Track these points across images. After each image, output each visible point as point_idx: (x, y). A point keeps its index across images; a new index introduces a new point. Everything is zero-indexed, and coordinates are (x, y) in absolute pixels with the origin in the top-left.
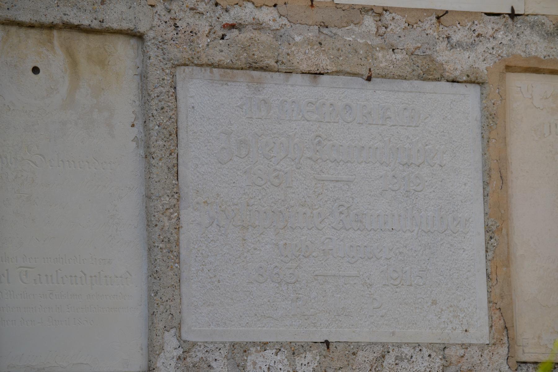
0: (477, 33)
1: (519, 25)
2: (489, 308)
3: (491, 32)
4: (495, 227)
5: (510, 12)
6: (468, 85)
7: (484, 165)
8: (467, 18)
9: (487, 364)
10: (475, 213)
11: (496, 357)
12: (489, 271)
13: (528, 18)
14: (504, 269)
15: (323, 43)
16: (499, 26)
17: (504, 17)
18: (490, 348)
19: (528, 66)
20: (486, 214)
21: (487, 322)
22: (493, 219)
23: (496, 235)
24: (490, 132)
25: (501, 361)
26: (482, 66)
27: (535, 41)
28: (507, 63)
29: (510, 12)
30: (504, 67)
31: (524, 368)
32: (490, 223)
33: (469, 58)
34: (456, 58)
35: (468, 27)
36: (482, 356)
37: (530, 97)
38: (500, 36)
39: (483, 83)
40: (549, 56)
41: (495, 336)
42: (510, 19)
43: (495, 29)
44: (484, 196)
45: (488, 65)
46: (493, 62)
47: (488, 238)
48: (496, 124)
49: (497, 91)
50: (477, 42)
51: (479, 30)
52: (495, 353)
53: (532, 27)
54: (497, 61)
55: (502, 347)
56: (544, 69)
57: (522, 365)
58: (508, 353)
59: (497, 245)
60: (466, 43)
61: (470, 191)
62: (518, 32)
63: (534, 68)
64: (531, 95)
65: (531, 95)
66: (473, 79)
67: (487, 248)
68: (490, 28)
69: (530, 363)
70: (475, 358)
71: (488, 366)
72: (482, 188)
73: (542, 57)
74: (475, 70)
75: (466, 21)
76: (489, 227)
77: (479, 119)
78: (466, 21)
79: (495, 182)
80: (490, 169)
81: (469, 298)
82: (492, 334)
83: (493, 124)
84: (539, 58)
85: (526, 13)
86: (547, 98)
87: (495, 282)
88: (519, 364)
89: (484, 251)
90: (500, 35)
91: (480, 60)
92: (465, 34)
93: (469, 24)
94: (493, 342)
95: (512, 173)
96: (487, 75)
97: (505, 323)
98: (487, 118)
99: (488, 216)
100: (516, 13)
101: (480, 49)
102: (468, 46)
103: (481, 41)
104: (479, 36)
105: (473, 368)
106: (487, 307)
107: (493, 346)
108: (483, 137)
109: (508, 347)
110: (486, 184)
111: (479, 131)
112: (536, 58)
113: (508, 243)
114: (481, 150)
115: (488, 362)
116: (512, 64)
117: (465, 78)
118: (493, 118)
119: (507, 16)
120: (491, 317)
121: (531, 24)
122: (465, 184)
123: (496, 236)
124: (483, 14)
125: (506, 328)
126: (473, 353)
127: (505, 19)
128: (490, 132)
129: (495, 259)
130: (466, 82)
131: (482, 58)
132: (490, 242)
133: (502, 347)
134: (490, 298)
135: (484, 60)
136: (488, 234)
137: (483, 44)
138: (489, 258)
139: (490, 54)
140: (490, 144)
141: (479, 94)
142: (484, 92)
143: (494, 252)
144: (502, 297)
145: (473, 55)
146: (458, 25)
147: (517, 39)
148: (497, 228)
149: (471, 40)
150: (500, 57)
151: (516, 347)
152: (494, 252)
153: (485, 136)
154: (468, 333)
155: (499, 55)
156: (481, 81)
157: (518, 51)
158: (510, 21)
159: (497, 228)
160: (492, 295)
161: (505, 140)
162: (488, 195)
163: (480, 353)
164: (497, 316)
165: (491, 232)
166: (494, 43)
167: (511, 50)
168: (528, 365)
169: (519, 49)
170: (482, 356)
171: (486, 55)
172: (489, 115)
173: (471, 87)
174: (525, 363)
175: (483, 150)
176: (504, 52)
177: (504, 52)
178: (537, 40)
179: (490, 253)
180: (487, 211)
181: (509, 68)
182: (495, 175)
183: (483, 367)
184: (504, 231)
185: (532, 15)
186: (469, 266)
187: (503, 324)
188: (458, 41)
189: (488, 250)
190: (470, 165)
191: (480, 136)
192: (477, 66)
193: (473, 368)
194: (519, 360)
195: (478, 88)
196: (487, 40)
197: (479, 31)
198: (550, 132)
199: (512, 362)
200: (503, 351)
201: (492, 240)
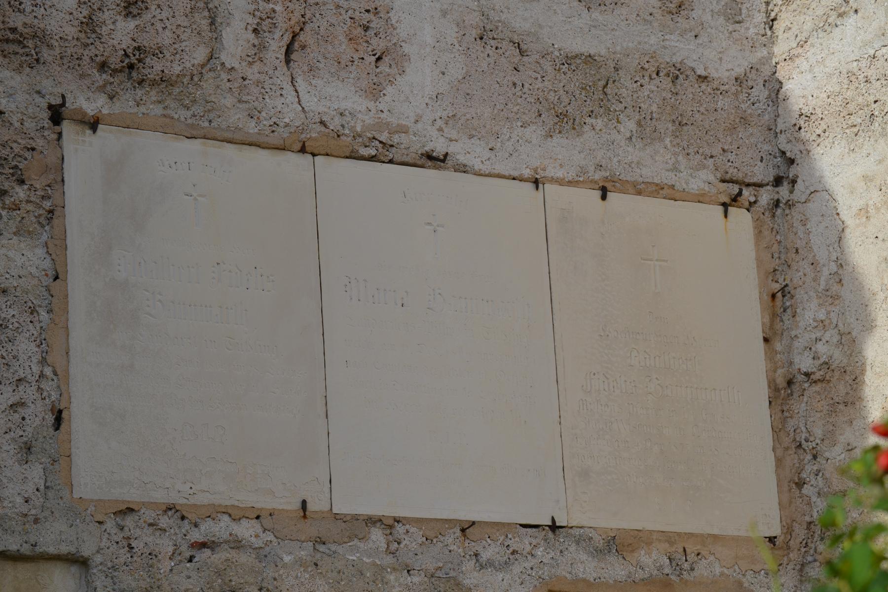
0: (511, 550)
1: (562, 540)
3: (528, 548)
8: (498, 530)
15: (696, 552)
16: (538, 540)
28: (549, 587)
29: (550, 524)
50: (512, 561)
53: (578, 543)
60: (499, 561)
73: (592, 580)
85: (570, 525)
90: (539, 552)
93: (502, 538)
100: (557, 524)
101: (517, 569)
103: (516, 560)
112: (584, 580)
119: (547, 528)
131: (519, 581)
145: (508, 576)
146: (488, 540)
149: (505, 558)
157: (563, 571)
158: (550, 535)
166: (532, 562)
176: (546, 573)
197: (514, 547)
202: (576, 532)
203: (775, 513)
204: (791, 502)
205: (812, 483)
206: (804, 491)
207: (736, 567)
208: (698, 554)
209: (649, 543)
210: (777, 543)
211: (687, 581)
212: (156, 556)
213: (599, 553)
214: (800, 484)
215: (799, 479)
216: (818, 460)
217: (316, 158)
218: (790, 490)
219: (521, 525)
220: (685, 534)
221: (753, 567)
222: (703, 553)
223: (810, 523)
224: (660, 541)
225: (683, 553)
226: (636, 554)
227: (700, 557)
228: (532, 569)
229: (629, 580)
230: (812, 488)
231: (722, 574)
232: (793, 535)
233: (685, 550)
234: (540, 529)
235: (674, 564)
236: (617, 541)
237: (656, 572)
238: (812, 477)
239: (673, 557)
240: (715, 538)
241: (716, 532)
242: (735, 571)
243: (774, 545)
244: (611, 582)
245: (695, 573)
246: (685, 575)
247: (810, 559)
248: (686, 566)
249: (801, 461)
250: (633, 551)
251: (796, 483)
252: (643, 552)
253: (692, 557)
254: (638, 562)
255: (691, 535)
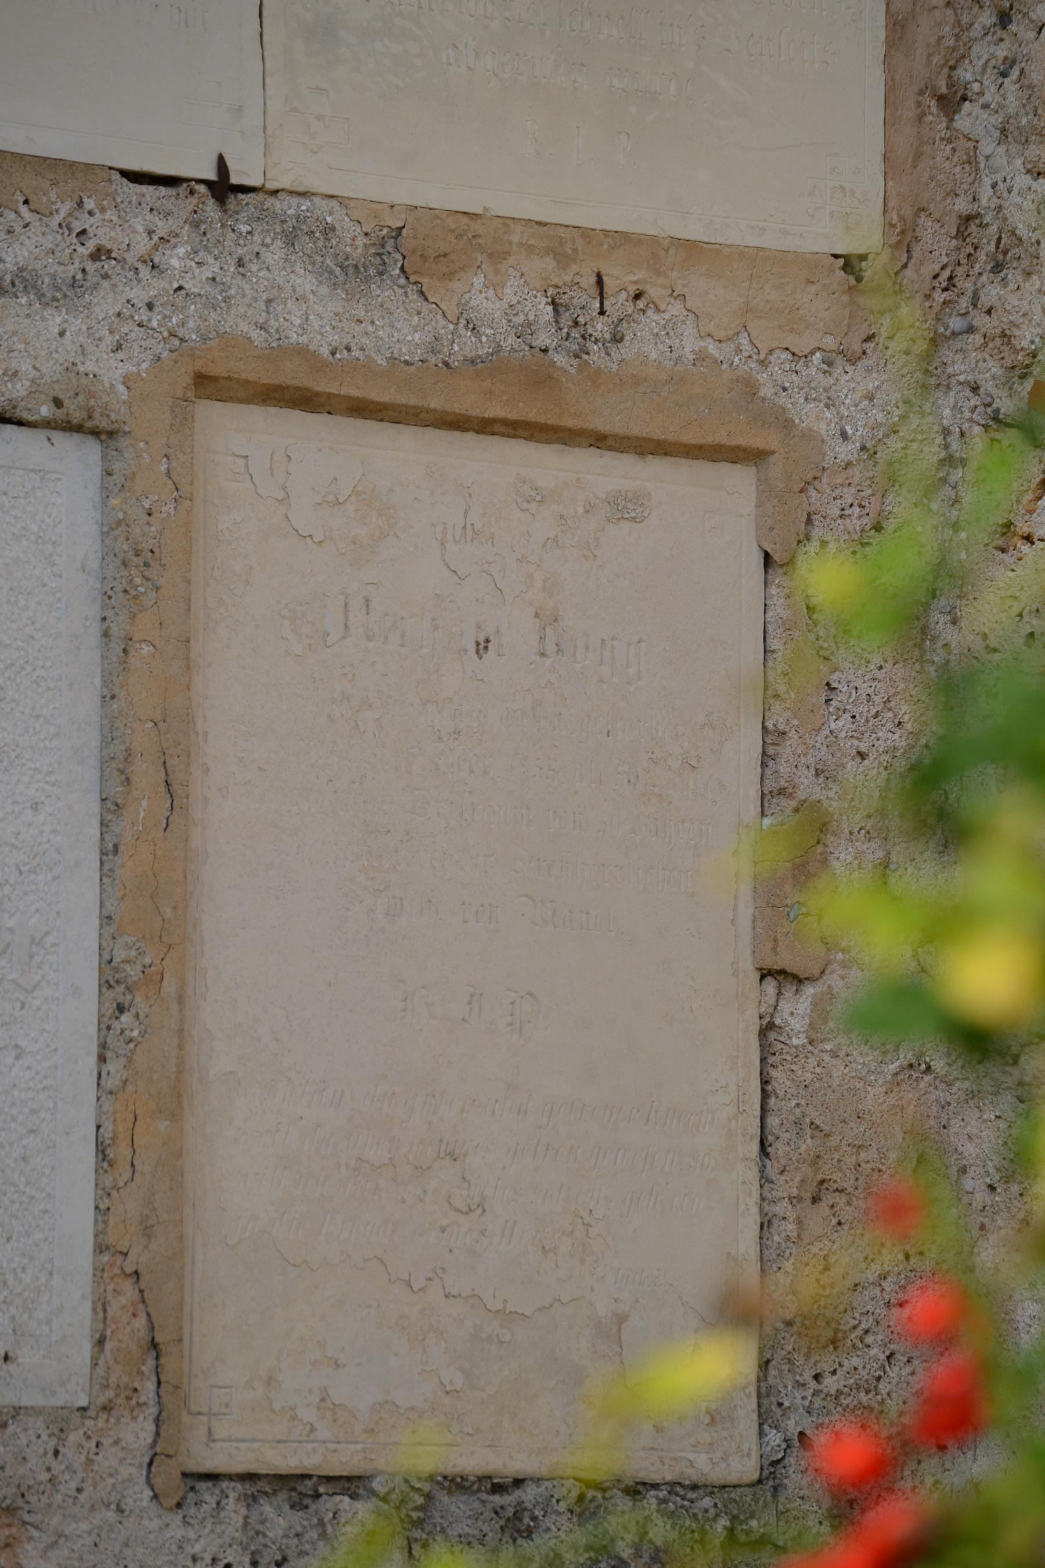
0: (91, 245)
1: (244, 229)
2: (99, 1271)
3: (142, 245)
4: (139, 967)
5: (212, 175)
6: (57, 436)
7: (108, 739)
8: (54, 184)
9: (73, 1485)
10: (69, 918)
11: (109, 1458)
12: (107, 1131)
13: (276, 204)
14: (163, 1125)
15: (632, 290)
16: (173, 224)
17: (192, 192)
18: (90, 1423)
19: (276, 382)
20: (107, 919)
21: (88, 1324)
22: (130, 940)
23: (138, 999)
24: (133, 617)
25: (125, 1471)
26: (111, 371)
27: (300, 291)
28: (199, 365)
29: (212, 175)
30: (188, 380)
31: (207, 1497)
32: (120, 954)
33: (62, 334)
34: (15, 333)
35: (58, 219)
36: (56, 1453)
37: (281, 495)
38: (175, 262)
39: (111, 434)
40: (348, 349)
41: (113, 1379)
42: (211, 201)
43: (160, 233)
44: (103, 853)
45: (130, 368)
46: (149, 356)
47: (110, 1008)
48: (158, 588)
49: (163, 468)
50: (93, 279)
51: (100, 232)
52: (106, 1442)
53: (290, 240)
54: (165, 354)
55: (134, 1419)
56: (330, 396)
57: (202, 1486)
58: (155, 1442)
59: (142, 1034)
60: (54, 277)
61: (54, 832)
62: (240, 251)
63: (297, 389)
64: (284, 487)
65: (284, 487)
66: (77, 417)
67: (103, 1046)
68: (140, 228)
69: (230, 1477)
70: (34, 1461)
71: (79, 1490)
72: (95, 822)
73: (325, 352)
74: (84, 381)
75: (53, 195)
76: (117, 970)
77: (94, 564)
78: (53, 195)
79: (144, 803)
80: (129, 753)
81: (27, 1234)
82: (101, 1371)
83: (146, 584)
84: (315, 355)
85: (271, 186)
86: (338, 503)
87: (128, 1175)
88: (190, 1482)
89: (94, 1058)
90: (175, 259)
91: (103, 346)
92: (48, 243)
93: (65, 208)
94: (102, 1400)
95: (207, 770)
96: (128, 404)
97: (152, 1328)
98: (125, 564)
99: (112, 929)
100: (234, 180)
101: (105, 304)
102: (58, 289)
103: (106, 276)
104: (99, 254)
105: (20, 1502)
106: (89, 1268)
107: (104, 1416)
108: (106, 634)
109: (157, 1421)
110: (111, 809)
111: (95, 611)
112: (302, 351)
113: (181, 1030)
114: (98, 680)
115: (80, 1475)
116: (218, 370)
117: (46, 411)
118: (146, 565)
119: (202, 189)
120: (101, 1306)
121: (288, 226)
122: (35, 807)
123: (141, 1005)
124: (116, 176)
125: (154, 1345)
126: (24, 1441)
127: (193, 201)
128: (133, 617)
129: (130, 1088)
130: (48, 424)
131: (109, 340)
132: (117, 1026)
133: (134, 1419)
134: (104, 1232)
135: (118, 348)
136: (110, 994)
137: (114, 286)
138: (109, 1083)
139: (140, 325)
140: (133, 660)
141: (98, 472)
142: (116, 466)
143: (130, 1060)
144: (147, 1231)
145: (77, 324)
146: (24, 210)
147: (238, 280)
148: (143, 978)
149: (73, 269)
150: (176, 342)
151: (186, 1418)
152: (130, 1060)
153: (114, 631)
154: (11, 1367)
155: (172, 335)
156: (104, 424)
157: (241, 321)
158: (211, 209)
159: (143, 978)
160: (112, 1222)
161: (188, 649)
162: (116, 849)
163: (53, 1442)
164: (123, 1300)
165: (121, 988)
166: (155, 287)
167: (214, 316)
168: (225, 1484)
169: (245, 316)
170: (56, 1453)
171: (125, 329)
172: (130, 555)
173: (66, 444)
174: (213, 1477)
175: (106, 682)
176: (191, 322)
177: (191, 324)
178: (308, 287)
179: (113, 1066)
180: (110, 908)
181: (206, 385)
182: (146, 775)
183: (58, 1498)
184: (169, 986)
185: (291, 193)
186: (33, 1112)
187: (144, 1334)
188: (22, 270)
189: (109, 1054)
190: (57, 735)
191: (96, 628)
192: (90, 367)
193: (20, 1502)
194: (192, 1467)
195: (92, 449)
196: (131, 274)
197: (101, 236)
198: (346, 626)
199: (168, 1475)
200: (138, 1433)
201: (124, 1018)
202: (289, 207)
203: (870, 182)
204: (918, 155)
205: (988, 97)
206: (962, 122)
207: (744, 340)
208: (638, 296)
209: (498, 256)
210: (867, 274)
211: (599, 371)
212: (19, 1486)
213: (350, 274)
214: (952, 101)
215: (950, 85)
216: (1013, 27)
217: (407, 1278)
218: (920, 118)
219: (125, 174)
220: (606, 233)
221: (789, 341)
222: (653, 292)
223: (969, 218)
224: (531, 250)
225: (594, 291)
226: (458, 286)
227: (641, 304)
228: (150, 306)
229: (433, 360)
230: (984, 115)
231: (701, 357)
232: (916, 252)
233: (600, 282)
234: (183, 189)
235: (566, 320)
236: (407, 241)
237: (511, 340)
238: (990, 80)
239: (564, 299)
240: (692, 251)
241: (694, 231)
242: (738, 351)
243: (859, 279)
244: (381, 361)
245: (626, 351)
246: (595, 354)
247: (956, 323)
248: (600, 327)
249: (962, 28)
250: (450, 276)
251: (941, 99)
252: (478, 281)
253: (618, 303)
254: (463, 308)
255: (622, 238)
